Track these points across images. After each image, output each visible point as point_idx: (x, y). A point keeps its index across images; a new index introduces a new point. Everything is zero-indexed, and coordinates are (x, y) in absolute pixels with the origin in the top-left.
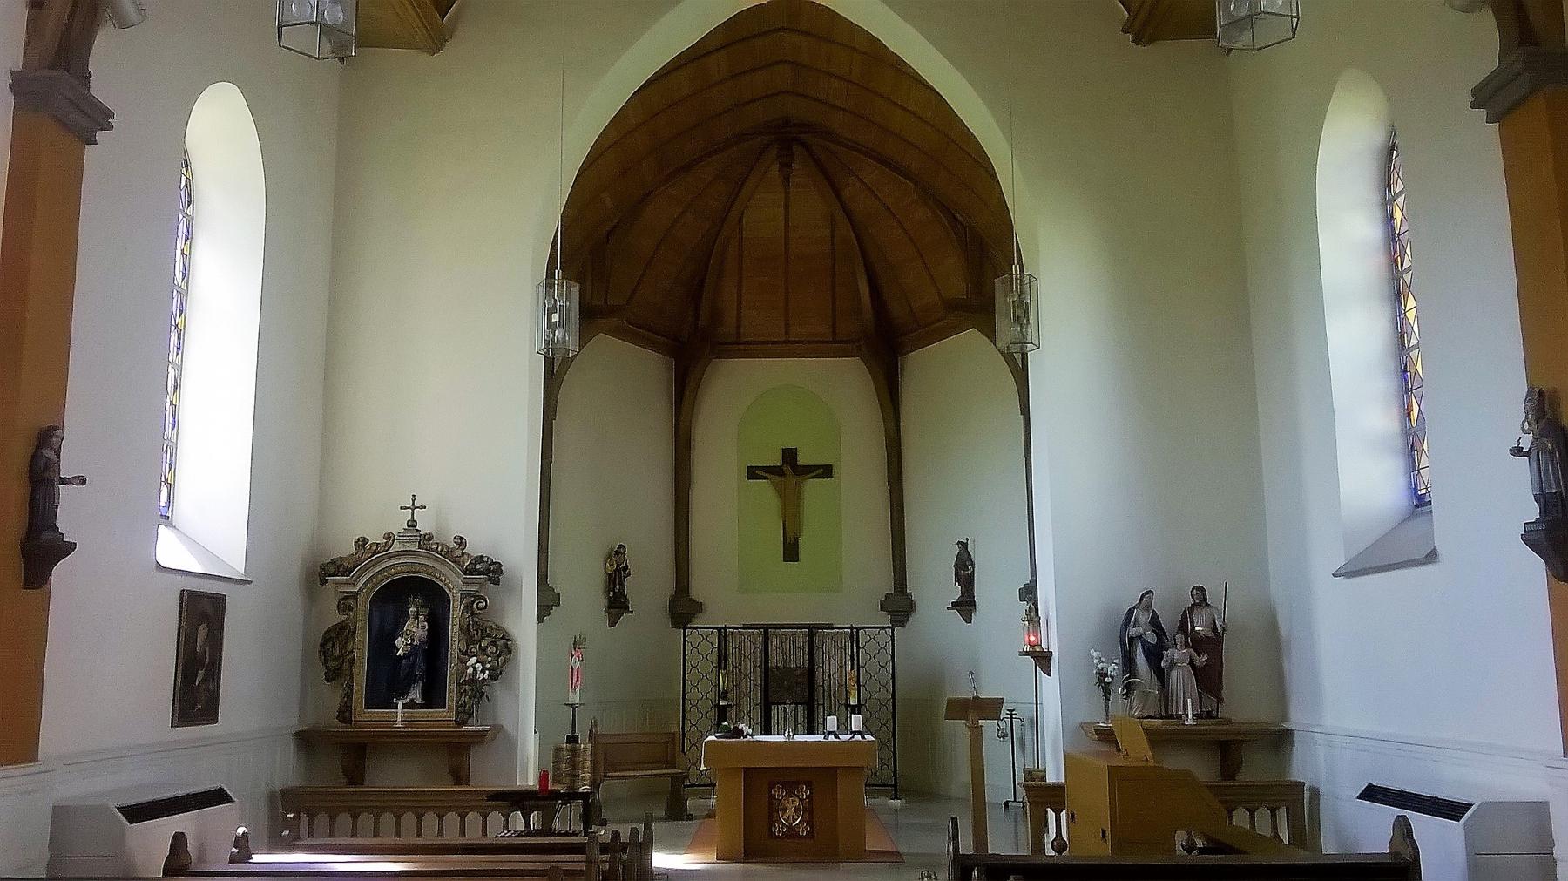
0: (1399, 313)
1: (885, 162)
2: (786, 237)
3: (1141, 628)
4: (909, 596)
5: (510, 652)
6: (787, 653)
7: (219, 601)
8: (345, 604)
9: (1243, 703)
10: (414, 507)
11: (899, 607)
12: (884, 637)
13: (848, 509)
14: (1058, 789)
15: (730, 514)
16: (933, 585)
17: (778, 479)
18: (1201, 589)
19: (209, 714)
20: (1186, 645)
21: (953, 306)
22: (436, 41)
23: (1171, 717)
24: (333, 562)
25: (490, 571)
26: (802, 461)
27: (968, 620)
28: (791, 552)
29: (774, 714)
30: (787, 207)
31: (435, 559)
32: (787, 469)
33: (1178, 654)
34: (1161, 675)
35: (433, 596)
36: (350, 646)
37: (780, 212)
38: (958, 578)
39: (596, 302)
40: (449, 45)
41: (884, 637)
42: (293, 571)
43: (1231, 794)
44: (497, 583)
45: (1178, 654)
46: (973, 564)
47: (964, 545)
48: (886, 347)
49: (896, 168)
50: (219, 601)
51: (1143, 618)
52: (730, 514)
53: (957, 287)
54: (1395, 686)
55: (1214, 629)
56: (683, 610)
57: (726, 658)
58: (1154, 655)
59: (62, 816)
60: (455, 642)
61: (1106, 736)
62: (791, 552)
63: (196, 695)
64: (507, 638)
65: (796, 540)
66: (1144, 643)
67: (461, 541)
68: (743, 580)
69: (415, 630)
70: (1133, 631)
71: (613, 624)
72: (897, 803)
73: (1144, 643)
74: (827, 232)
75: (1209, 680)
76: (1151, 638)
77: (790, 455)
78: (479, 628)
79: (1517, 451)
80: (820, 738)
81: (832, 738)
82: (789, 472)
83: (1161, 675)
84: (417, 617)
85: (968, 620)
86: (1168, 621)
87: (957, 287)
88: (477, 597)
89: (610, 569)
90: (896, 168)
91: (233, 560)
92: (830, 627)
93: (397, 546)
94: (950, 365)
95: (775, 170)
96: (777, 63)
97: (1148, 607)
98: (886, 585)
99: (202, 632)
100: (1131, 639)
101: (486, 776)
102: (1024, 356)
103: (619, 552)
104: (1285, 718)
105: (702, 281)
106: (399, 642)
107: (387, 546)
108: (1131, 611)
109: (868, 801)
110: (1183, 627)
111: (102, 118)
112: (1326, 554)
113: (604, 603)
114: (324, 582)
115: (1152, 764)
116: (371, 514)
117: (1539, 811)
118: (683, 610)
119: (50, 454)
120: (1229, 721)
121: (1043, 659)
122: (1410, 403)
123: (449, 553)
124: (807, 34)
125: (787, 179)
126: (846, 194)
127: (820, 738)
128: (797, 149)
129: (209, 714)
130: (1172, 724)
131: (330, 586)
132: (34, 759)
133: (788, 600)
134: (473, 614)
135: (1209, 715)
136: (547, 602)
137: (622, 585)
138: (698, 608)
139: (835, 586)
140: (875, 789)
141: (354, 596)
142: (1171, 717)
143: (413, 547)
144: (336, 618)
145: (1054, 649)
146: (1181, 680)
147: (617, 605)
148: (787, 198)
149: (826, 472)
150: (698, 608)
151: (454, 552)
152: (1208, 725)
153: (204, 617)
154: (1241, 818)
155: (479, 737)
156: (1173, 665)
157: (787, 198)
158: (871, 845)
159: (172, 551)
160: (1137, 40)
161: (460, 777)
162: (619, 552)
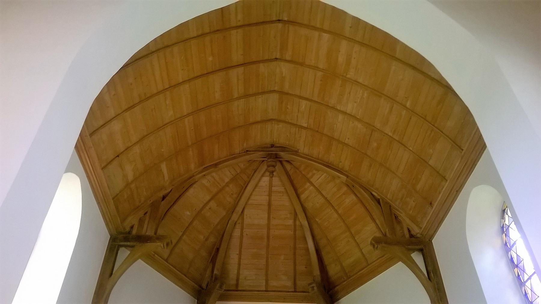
74: (291, 222)
105: (218, 250)
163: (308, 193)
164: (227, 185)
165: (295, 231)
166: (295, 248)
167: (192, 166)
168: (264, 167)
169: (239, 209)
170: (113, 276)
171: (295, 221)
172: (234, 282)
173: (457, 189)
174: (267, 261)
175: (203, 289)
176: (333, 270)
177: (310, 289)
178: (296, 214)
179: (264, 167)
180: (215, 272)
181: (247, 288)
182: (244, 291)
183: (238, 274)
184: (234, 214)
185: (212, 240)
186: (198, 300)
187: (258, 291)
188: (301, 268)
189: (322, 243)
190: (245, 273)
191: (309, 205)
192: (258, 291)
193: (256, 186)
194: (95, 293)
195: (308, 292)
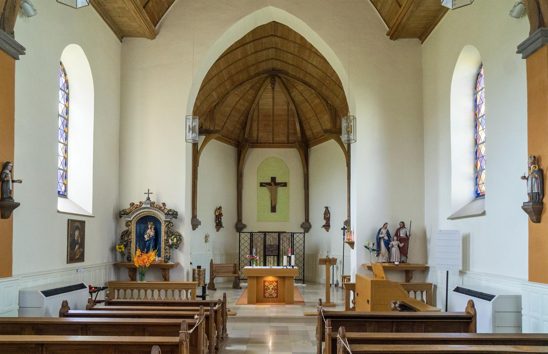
0: (476, 132)
1: (305, 83)
2: (273, 109)
3: (383, 235)
4: (310, 224)
5: (181, 240)
6: (271, 240)
7: (83, 223)
8: (128, 224)
9: (414, 258)
10: (149, 193)
11: (307, 226)
12: (301, 236)
14: (354, 285)
15: (255, 198)
17: (270, 187)
18: (403, 223)
19: (81, 259)
20: (397, 240)
21: (326, 131)
22: (153, 35)
23: (391, 262)
24: (123, 210)
25: (174, 214)
26: (278, 181)
27: (328, 231)
28: (273, 209)
29: (267, 259)
30: (273, 98)
31: (156, 210)
32: (272, 183)
33: (395, 243)
34: (389, 249)
35: (156, 221)
36: (130, 237)
37: (272, 100)
39: (211, 129)
40: (158, 37)
41: (301, 236)
42: (110, 212)
43: (408, 287)
44: (176, 218)
45: (395, 243)
47: (327, 208)
48: (305, 145)
49: (310, 86)
50: (83, 223)
51: (384, 231)
52: (255, 198)
53: (328, 125)
54: (486, 261)
55: (406, 235)
56: (240, 227)
58: (387, 244)
59: (22, 294)
60: (163, 237)
61: (370, 268)
62: (273, 209)
63: (76, 252)
64: (180, 235)
65: (275, 206)
66: (384, 240)
67: (164, 204)
68: (258, 218)
69: (150, 232)
70: (381, 236)
71: (218, 231)
72: (304, 285)
73: (384, 240)
74: (286, 107)
75: (404, 251)
76: (386, 238)
77: (273, 179)
78: (171, 232)
79: (524, 178)
80: (281, 267)
81: (285, 267)
82: (273, 184)
83: (389, 249)
84: (151, 228)
85: (328, 231)
86: (392, 233)
87: (328, 125)
88: (170, 222)
89: (217, 214)
90: (310, 86)
91: (89, 210)
92: (285, 232)
93: (144, 206)
94: (326, 151)
95: (269, 87)
96: (270, 48)
97: (386, 228)
99: (77, 233)
100: (380, 238)
101: (175, 277)
102: (349, 145)
103: (220, 208)
104: (427, 263)
105: (246, 123)
106: (146, 236)
107: (140, 206)
108: (380, 230)
109: (295, 284)
110: (397, 234)
111: (21, 50)
112: (445, 212)
113: (215, 225)
114: (121, 217)
115: (385, 279)
116: (136, 196)
117: (518, 299)
118: (240, 227)
119: (8, 172)
120: (409, 264)
121: (352, 244)
122: (477, 162)
123: (160, 208)
124: (280, 37)
125: (273, 88)
126: (292, 94)
127: (281, 267)
128: (277, 79)
129: (81, 259)
130: (391, 265)
131: (123, 218)
132: (11, 276)
133: (273, 224)
134: (169, 228)
135: (403, 262)
136: (195, 224)
137: (221, 219)
138: (245, 226)
139: (288, 221)
140: (297, 280)
141: (131, 221)
142: (391, 262)
143: (149, 206)
144: (126, 228)
145: (355, 241)
146: (395, 251)
147: (219, 225)
148: (273, 95)
149: (285, 185)
150: (245, 226)
151: (162, 208)
152: (403, 265)
153: (77, 228)
154: (412, 294)
155: (172, 266)
156: (393, 246)
157: (273, 95)
158: (295, 300)
159: (62, 205)
160: (391, 38)
161: (166, 278)
162: (220, 208)
163: (295, 93)
164: (248, 90)
165: (288, 112)
166: (288, 121)
167: (228, 87)
168: (269, 80)
169: (256, 102)
170: (213, 217)
171: (288, 107)
172: (255, 138)
173: (324, 222)
174: (273, 128)
176: (308, 133)
178: (288, 103)
179: (269, 80)
180: (246, 136)
182: (261, 143)
183: (258, 135)
184: (254, 105)
185: (242, 118)
188: (291, 131)
189: (303, 119)
190: (261, 134)
191: (296, 99)
193: (265, 89)
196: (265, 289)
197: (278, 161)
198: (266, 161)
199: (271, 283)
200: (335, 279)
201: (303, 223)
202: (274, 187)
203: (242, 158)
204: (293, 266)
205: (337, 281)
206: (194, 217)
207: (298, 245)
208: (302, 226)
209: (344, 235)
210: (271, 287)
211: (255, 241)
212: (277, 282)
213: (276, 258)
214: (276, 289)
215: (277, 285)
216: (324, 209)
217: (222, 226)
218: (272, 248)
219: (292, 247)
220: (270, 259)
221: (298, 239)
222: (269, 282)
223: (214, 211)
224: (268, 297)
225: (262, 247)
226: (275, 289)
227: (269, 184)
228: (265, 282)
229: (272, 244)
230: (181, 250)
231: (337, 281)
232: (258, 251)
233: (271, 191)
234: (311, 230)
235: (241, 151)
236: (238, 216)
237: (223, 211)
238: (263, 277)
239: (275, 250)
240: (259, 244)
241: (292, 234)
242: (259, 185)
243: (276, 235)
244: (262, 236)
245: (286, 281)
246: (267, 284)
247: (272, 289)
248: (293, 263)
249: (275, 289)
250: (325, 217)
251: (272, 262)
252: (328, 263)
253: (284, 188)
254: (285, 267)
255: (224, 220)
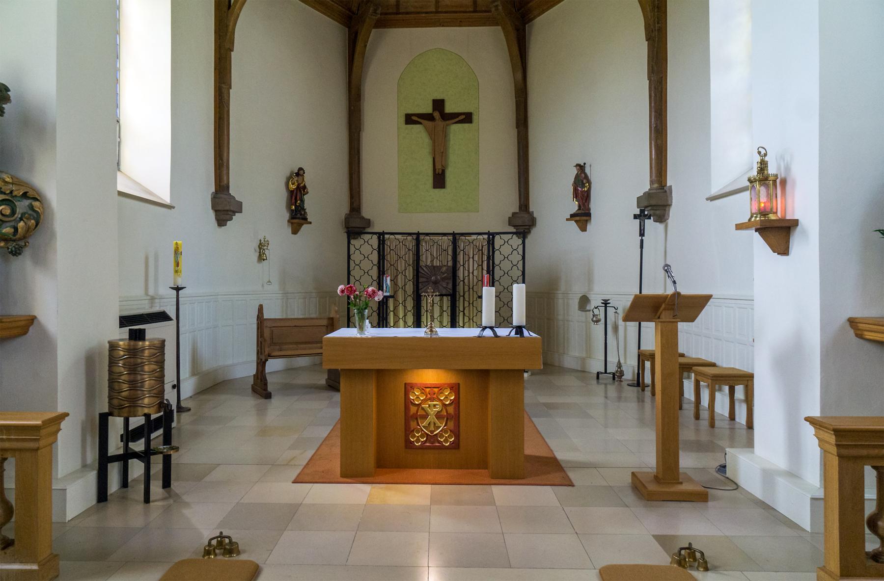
4: (531, 214)
6: (434, 256)
11: (523, 223)
13: (484, 148)
15: (393, 151)
16: (553, 200)
17: (429, 124)
26: (449, 108)
27: (583, 229)
28: (439, 180)
29: (424, 303)
32: (437, 115)
38: (576, 194)
46: (589, 182)
47: (581, 168)
52: (393, 151)
56: (355, 226)
57: (384, 259)
62: (439, 180)
64: (32, 196)
65: (443, 172)
68: (400, 201)
71: (295, 232)
77: (439, 104)
80: (472, 332)
81: (488, 333)
85: (583, 229)
89: (293, 187)
98: (513, 206)
103: (300, 173)
113: (287, 216)
118: (355, 226)
127: (472, 332)
133: (436, 215)
137: (302, 201)
139: (483, 205)
147: (297, 216)
149: (467, 118)
150: (368, 223)
162: (300, 173)
170: (281, 197)
175: (353, 13)
177: (493, 9)
181: (413, 10)
182: (407, 13)
186: (349, 27)
187: (427, 13)
192: (427, 13)
194: (215, 32)
195: (489, 11)
196: (412, 416)
197: (453, 59)
198: (419, 60)
199: (432, 391)
200: (612, 359)
201: (514, 214)
202: (440, 123)
203: (359, 48)
204: (519, 330)
205: (619, 365)
206: (221, 187)
207: (506, 265)
208: (510, 224)
209: (642, 234)
210: (433, 408)
211: (390, 257)
212: (455, 388)
213: (446, 301)
214: (453, 416)
215: (456, 403)
216: (575, 171)
217: (306, 219)
218: (440, 278)
219: (491, 271)
220: (431, 301)
221: (506, 250)
222: (423, 388)
223: (284, 180)
224: (421, 448)
225: (410, 273)
226: (448, 418)
227: (428, 117)
228: (409, 388)
229: (437, 263)
230: (41, 261)
231: (619, 365)
232: (400, 283)
233: (432, 135)
234: (534, 231)
235: (356, 34)
236: (352, 196)
237: (309, 179)
238: (401, 371)
239: (443, 279)
240: (401, 266)
241: (491, 236)
242: (403, 119)
243: (446, 241)
244: (410, 242)
245: (494, 389)
246: (416, 396)
247: (438, 416)
248: (519, 316)
249: (448, 418)
250: (575, 191)
251: (437, 314)
252: (666, 316)
253: (466, 125)
254: (488, 333)
255: (310, 203)
